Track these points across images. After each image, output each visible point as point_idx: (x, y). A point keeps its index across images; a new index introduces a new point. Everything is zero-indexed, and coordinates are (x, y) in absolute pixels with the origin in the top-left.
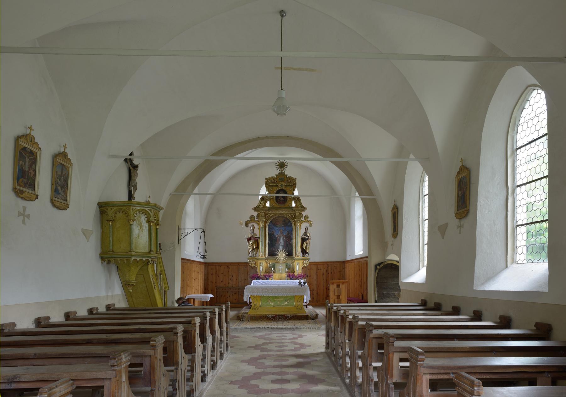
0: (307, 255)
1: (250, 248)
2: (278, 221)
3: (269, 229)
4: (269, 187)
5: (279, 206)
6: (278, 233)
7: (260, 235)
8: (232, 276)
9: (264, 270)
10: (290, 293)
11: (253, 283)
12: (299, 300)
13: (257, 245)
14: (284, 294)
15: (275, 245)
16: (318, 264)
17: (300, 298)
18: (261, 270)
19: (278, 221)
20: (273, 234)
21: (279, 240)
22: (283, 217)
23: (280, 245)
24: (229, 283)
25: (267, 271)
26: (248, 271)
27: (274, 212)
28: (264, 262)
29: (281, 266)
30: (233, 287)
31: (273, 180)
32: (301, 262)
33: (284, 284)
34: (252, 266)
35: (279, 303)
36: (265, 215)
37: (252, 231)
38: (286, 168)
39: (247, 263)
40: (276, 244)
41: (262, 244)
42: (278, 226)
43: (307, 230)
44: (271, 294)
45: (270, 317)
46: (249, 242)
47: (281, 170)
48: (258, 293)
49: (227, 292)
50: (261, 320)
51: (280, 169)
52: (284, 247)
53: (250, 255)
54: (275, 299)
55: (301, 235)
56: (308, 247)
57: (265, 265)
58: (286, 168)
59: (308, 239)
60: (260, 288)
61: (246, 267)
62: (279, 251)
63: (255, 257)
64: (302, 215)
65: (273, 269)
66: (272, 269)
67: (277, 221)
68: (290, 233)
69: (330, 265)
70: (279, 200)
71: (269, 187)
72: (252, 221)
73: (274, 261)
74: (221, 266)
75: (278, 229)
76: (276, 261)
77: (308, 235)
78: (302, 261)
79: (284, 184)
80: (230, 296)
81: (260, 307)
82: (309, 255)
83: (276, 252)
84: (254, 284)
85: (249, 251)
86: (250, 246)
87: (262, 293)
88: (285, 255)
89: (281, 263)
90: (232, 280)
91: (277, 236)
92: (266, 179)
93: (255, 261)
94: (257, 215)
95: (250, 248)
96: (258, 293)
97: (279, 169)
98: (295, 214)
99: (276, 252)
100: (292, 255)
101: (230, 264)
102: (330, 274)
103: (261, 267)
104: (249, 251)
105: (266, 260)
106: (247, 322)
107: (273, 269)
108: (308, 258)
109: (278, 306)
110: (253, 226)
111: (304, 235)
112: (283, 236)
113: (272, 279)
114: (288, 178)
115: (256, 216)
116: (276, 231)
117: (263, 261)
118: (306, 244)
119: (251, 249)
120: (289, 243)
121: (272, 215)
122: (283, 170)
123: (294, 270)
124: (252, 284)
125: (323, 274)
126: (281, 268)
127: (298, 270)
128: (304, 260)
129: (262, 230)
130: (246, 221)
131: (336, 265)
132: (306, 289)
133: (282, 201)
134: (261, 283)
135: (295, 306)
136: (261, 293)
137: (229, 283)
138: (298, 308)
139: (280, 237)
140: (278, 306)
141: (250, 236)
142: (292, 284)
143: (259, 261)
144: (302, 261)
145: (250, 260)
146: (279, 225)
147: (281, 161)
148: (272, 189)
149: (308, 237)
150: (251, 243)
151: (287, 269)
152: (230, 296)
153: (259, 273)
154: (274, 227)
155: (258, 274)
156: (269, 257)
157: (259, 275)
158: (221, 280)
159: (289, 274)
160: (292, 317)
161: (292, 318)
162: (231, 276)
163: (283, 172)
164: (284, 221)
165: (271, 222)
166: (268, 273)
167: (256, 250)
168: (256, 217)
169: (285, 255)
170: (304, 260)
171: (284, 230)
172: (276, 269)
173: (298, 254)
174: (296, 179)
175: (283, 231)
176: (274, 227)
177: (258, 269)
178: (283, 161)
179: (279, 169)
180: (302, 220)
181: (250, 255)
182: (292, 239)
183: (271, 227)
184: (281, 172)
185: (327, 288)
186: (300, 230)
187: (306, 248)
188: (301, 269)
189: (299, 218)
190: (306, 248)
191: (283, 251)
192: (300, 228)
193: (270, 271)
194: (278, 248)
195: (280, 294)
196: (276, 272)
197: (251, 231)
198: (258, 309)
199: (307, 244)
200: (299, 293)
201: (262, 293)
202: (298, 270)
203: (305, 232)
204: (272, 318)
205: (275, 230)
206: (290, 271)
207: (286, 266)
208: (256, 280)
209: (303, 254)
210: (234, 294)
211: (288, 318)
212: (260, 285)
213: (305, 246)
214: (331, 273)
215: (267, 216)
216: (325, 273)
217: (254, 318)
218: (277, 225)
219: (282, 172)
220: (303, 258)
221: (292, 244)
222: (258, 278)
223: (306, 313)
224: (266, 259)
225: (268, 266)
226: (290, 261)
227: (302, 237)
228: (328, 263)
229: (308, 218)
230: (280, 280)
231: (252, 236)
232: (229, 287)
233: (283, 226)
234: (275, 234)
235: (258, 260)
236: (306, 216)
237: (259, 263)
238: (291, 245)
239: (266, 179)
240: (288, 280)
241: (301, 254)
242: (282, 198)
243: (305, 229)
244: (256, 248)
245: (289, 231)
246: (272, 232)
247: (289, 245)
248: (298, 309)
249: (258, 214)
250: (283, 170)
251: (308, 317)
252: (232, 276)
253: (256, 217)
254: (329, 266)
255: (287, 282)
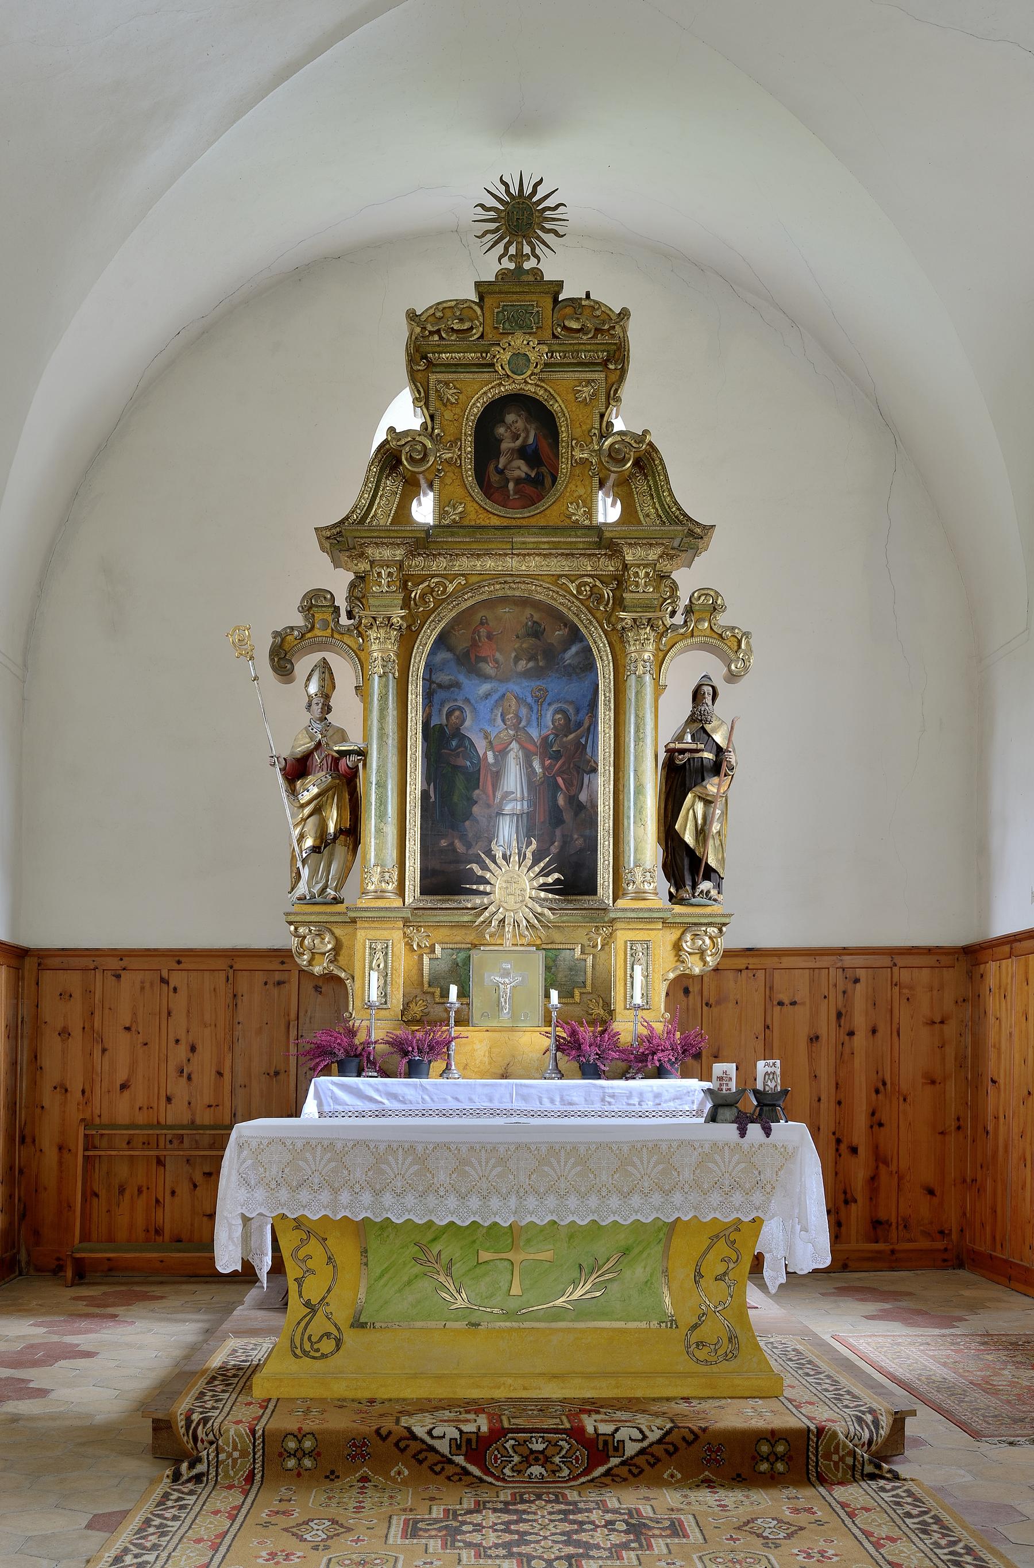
0: (705, 886)
1: (302, 837)
2: (490, 637)
3: (429, 696)
4: (433, 378)
5: (495, 521)
6: (492, 722)
7: (367, 736)
8: (193, 1049)
9: (397, 1001)
10: (626, 1196)
11: (317, 1096)
12: (713, 1266)
13: (347, 815)
14: (572, 1202)
15: (468, 815)
16: (770, 962)
17: (722, 1248)
18: (374, 996)
19: (490, 637)
20: (457, 734)
21: (497, 776)
22: (524, 602)
23: (499, 814)
24: (169, 1100)
25: (416, 1009)
26: (293, 1015)
27: (464, 564)
28: (396, 936)
29: (506, 974)
30: (192, 1125)
31: (461, 320)
32: (663, 939)
33: (535, 1106)
34: (317, 970)
35: (516, 1290)
36: (405, 583)
37: (317, 709)
38: (548, 238)
39: (283, 956)
40: (475, 809)
41: (382, 802)
42: (488, 669)
43: (709, 699)
44: (452, 1202)
45: (443, 1447)
46: (293, 792)
47: (512, 250)
48: (335, 1191)
49: (160, 1162)
50: (365, 1479)
51: (506, 249)
52: (529, 827)
53: (302, 888)
54: (485, 1256)
55: (666, 737)
56: (715, 828)
57: (402, 963)
58: (548, 238)
59: (716, 769)
60: (356, 1144)
61: (279, 983)
62: (499, 855)
63: (336, 901)
64: (674, 587)
65: (454, 990)
66: (445, 994)
67: (483, 631)
68: (579, 725)
69: (861, 974)
70: (495, 478)
71: (433, 378)
72: (317, 632)
73: (459, 935)
74: (118, 977)
75: (487, 696)
76: (471, 937)
77: (719, 738)
78: (673, 935)
79: (537, 353)
80: (173, 1193)
81: (358, 1324)
82: (718, 887)
83: (475, 867)
84: (320, 1105)
85: (293, 857)
86: (304, 820)
87: (377, 1193)
88: (543, 887)
89: (508, 944)
90: (189, 1078)
91: (481, 745)
92: (412, 316)
93: (338, 932)
94: (352, 586)
95: (302, 837)
96: (335, 1191)
97: (500, 248)
98: (620, 581)
99: (475, 867)
100: (591, 889)
101: (179, 957)
102: (860, 1040)
103: (374, 975)
104: (293, 857)
105: (406, 923)
106: (224, 1500)
107: (454, 990)
108: (716, 909)
109: (508, 1315)
110: (325, 667)
111: (688, 738)
112: (522, 747)
113: (448, 1067)
114: (568, 311)
115: (345, 594)
116: (474, 710)
117: (385, 934)
118: (700, 807)
119: (309, 842)
120: (573, 800)
121: (450, 588)
122: (527, 249)
123: (607, 1006)
124: (310, 1107)
125: (814, 1039)
126: (507, 984)
127: (638, 1000)
128: (687, 927)
129: (384, 698)
130: (276, 634)
131: (905, 976)
132: (788, 1155)
133: (518, 481)
134: (371, 1099)
135: (673, 1322)
136: (367, 1198)
137: (169, 1100)
138: (700, 1344)
139: (502, 753)
140: (508, 1315)
141: (304, 745)
142: (597, 1106)
143: (361, 934)
144: (673, 935)
145: (304, 923)
146: (496, 662)
147: (514, 190)
148: (449, 394)
149: (719, 750)
150: (305, 797)
151: (554, 994)
152: (173, 1193)
153: (358, 1019)
154: (462, 678)
155: (352, 1033)
156: (429, 901)
157: (360, 1038)
158: (121, 1076)
159: (573, 1033)
160: (658, 1450)
161: (655, 1462)
162: (182, 1050)
163: (527, 266)
164: (536, 632)
165: (442, 641)
166: (418, 1022)
167: (340, 850)
168: (342, 603)
169: (543, 887)
170: (687, 927)
171: (530, 700)
172: (474, 990)
173: (639, 878)
174: (625, 314)
175: (524, 711)
176: (462, 678)
177: (354, 988)
178: (528, 190)
179: (500, 248)
180: (674, 627)
181: (302, 888)
182: (594, 770)
183: (442, 678)
184: (512, 266)
185: (838, 1141)
186: (656, 701)
187: (701, 833)
188: (662, 989)
189: (648, 607)
190: (701, 833)
191: (522, 857)
192: (659, 689)
193: (437, 1011)
194: (490, 836)
195: (531, 1202)
196: (475, 1021)
197: (309, 706)
198: (339, 1343)
199: (708, 802)
200: (715, 1198)
201: (377, 1193)
202: (638, 1000)
203: (692, 719)
204: (460, 1460)
205: (467, 700)
206: (577, 1011)
207: (548, 968)
208: (342, 1072)
209: (679, 885)
210: (198, 1178)
211: (614, 1461)
212: (362, 1115)
213: (690, 825)
214: (874, 1031)
215: (416, 593)
216: (823, 1032)
217: (299, 1454)
218: (485, 660)
219: (519, 267)
220: (678, 909)
221: (595, 806)
222: (354, 1064)
223: (771, 1393)
224: (408, 914)
225: (421, 970)
226: (581, 935)
227: (671, 752)
228: (848, 961)
229: (714, 609)
230: (504, 1076)
231: (319, 745)
232: (171, 1127)
233: (527, 674)
234: (470, 728)
235: (354, 921)
236: (704, 592)
237: (358, 946)
238: (586, 815)
239: (412, 316)
240: (562, 1077)
241: (665, 886)
242: (521, 463)
243: (697, 695)
244: (340, 832)
245: (571, 710)
246: (449, 714)
247: (567, 816)
248: (702, 1354)
249: (361, 578)
250: (527, 249)
251: (828, 1456)
252: (193, 1049)
253: (342, 603)
254: (857, 981)
255: (561, 1090)
